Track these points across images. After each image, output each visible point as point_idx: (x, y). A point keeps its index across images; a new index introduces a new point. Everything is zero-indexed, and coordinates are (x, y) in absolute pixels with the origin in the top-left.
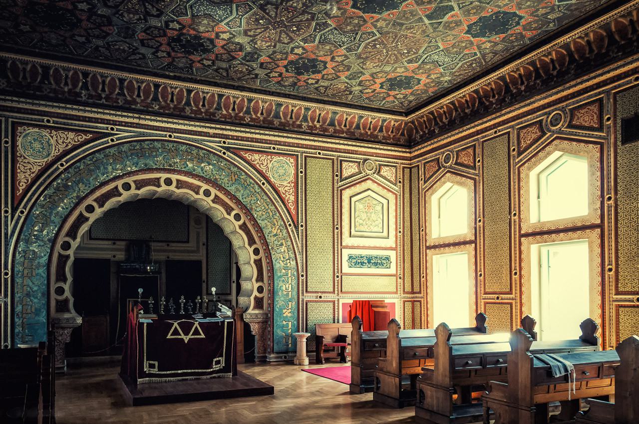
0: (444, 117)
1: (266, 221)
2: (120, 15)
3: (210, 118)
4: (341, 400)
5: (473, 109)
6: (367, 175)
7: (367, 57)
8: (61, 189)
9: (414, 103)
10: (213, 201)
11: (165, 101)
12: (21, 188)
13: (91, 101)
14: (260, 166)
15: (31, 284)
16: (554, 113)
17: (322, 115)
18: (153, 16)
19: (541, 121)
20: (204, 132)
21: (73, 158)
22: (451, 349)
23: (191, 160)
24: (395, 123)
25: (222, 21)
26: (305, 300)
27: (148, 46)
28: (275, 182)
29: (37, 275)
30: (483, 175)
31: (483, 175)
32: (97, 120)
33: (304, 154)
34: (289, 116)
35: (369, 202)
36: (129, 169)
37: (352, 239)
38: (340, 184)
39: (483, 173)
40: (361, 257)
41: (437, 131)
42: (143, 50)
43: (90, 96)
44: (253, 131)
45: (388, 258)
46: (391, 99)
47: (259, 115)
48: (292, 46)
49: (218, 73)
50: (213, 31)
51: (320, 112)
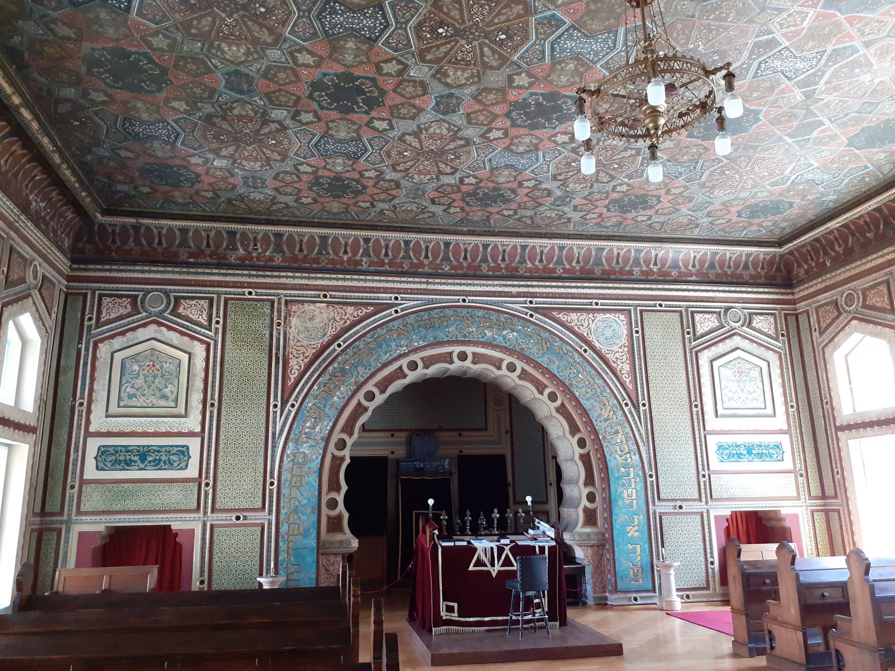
1: (592, 401)
3: (512, 275)
5: (876, 233)
6: (733, 330)
7: (714, 186)
9: (788, 230)
10: (520, 377)
11: (457, 260)
12: (293, 377)
13: (372, 269)
14: (579, 328)
15: (299, 495)
17: (660, 256)
18: (447, 174)
20: (504, 292)
21: (351, 336)
22: (872, 589)
23: (490, 328)
24: (766, 256)
25: (526, 169)
26: (658, 511)
27: (439, 204)
28: (601, 347)
29: (307, 483)
33: (639, 308)
34: (615, 261)
35: (739, 366)
36: (416, 344)
38: (694, 343)
40: (737, 446)
41: (828, 264)
42: (433, 208)
43: (372, 264)
44: (567, 284)
45: (778, 446)
46: (754, 228)
47: (574, 264)
48: (614, 184)
49: (522, 221)
51: (656, 252)
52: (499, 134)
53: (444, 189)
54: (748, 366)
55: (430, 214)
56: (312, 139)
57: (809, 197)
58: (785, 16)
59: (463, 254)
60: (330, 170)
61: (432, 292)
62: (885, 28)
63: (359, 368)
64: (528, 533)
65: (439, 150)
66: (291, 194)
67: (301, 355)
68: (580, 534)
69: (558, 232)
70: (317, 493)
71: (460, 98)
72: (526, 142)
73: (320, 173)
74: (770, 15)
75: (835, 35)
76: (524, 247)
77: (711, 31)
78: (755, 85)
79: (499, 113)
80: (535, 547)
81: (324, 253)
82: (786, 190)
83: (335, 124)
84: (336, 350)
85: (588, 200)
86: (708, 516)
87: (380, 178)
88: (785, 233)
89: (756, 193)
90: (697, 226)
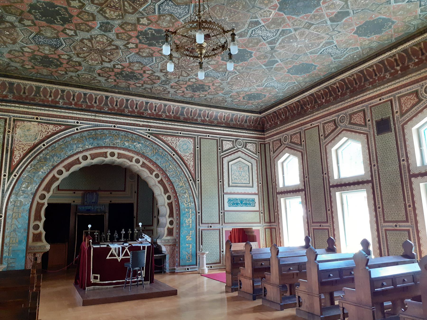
0: (282, 115)
2: (86, 61)
3: (140, 116)
4: (219, 296)
5: (297, 112)
6: (238, 149)
7: (233, 84)
8: (42, 160)
9: (264, 107)
10: (141, 166)
11: (112, 106)
12: (16, 160)
13: (65, 106)
14: (171, 144)
16: (341, 115)
17: (210, 114)
18: (106, 62)
19: (334, 121)
20: (136, 124)
24: (254, 118)
25: (147, 65)
26: (201, 229)
27: (103, 76)
28: (181, 153)
29: (22, 216)
30: (306, 150)
31: (306, 150)
32: (68, 118)
33: (199, 137)
34: (190, 114)
37: (230, 188)
39: (306, 149)
40: (237, 200)
41: (279, 123)
42: (99, 78)
45: (253, 200)
46: (250, 105)
47: (171, 113)
48: (189, 78)
49: (146, 90)
50: (142, 69)
52: (133, 46)
53: (105, 69)
54: (243, 165)
55: (98, 81)
56: (31, 35)
57: (272, 93)
58: (263, 12)
59: (115, 103)
60: (42, 52)
61: (98, 121)
62: (302, 24)
63: (55, 158)
64: (138, 240)
65: (102, 50)
66: (19, 62)
67: (22, 149)
68: (165, 240)
69: (164, 97)
70: (27, 222)
71: (113, 25)
72: (146, 52)
73: (36, 53)
74: (256, 10)
75: (283, 24)
76: (147, 103)
77: (231, 13)
78: (250, 40)
79: (133, 35)
80: (140, 247)
81: (38, 95)
82: (263, 89)
83: (44, 28)
84: (42, 147)
85: (177, 84)
86: (222, 231)
87: (70, 59)
88: (262, 108)
89: (251, 89)
90: (226, 101)
